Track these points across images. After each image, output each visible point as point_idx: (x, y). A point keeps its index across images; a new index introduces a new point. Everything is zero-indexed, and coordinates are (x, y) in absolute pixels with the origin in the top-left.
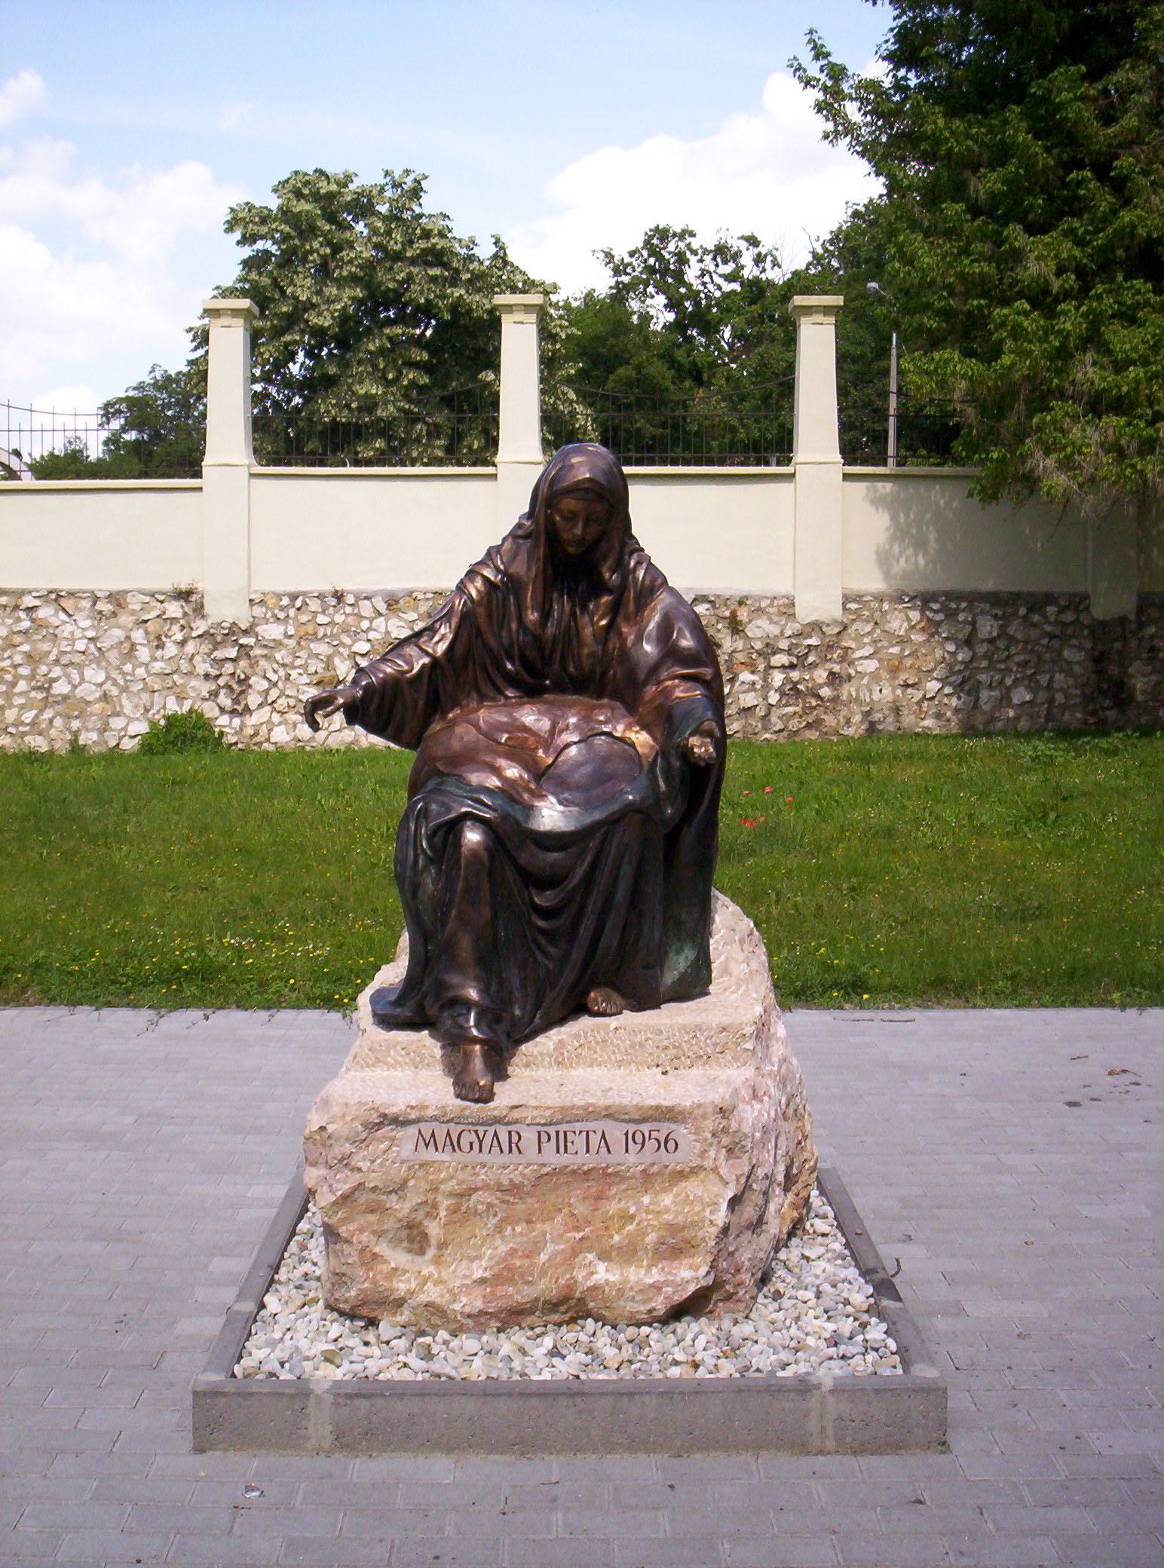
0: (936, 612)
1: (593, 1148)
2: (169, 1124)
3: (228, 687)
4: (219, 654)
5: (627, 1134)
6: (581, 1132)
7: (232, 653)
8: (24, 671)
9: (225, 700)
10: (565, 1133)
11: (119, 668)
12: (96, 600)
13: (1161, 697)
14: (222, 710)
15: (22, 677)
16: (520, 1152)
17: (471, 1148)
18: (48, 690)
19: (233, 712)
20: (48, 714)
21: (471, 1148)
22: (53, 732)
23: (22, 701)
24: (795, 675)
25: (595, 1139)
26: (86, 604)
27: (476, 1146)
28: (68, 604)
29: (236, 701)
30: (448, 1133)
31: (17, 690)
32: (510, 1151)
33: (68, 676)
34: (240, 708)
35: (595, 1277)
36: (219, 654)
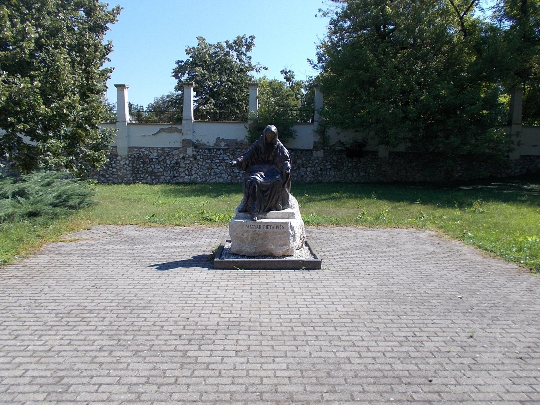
3: (187, 169)
4: (185, 162)
8: (142, 166)
9: (187, 173)
12: (158, 150)
14: (186, 175)
19: (189, 175)
20: (147, 175)
24: (313, 168)
26: (156, 151)
28: (152, 151)
36: (185, 162)
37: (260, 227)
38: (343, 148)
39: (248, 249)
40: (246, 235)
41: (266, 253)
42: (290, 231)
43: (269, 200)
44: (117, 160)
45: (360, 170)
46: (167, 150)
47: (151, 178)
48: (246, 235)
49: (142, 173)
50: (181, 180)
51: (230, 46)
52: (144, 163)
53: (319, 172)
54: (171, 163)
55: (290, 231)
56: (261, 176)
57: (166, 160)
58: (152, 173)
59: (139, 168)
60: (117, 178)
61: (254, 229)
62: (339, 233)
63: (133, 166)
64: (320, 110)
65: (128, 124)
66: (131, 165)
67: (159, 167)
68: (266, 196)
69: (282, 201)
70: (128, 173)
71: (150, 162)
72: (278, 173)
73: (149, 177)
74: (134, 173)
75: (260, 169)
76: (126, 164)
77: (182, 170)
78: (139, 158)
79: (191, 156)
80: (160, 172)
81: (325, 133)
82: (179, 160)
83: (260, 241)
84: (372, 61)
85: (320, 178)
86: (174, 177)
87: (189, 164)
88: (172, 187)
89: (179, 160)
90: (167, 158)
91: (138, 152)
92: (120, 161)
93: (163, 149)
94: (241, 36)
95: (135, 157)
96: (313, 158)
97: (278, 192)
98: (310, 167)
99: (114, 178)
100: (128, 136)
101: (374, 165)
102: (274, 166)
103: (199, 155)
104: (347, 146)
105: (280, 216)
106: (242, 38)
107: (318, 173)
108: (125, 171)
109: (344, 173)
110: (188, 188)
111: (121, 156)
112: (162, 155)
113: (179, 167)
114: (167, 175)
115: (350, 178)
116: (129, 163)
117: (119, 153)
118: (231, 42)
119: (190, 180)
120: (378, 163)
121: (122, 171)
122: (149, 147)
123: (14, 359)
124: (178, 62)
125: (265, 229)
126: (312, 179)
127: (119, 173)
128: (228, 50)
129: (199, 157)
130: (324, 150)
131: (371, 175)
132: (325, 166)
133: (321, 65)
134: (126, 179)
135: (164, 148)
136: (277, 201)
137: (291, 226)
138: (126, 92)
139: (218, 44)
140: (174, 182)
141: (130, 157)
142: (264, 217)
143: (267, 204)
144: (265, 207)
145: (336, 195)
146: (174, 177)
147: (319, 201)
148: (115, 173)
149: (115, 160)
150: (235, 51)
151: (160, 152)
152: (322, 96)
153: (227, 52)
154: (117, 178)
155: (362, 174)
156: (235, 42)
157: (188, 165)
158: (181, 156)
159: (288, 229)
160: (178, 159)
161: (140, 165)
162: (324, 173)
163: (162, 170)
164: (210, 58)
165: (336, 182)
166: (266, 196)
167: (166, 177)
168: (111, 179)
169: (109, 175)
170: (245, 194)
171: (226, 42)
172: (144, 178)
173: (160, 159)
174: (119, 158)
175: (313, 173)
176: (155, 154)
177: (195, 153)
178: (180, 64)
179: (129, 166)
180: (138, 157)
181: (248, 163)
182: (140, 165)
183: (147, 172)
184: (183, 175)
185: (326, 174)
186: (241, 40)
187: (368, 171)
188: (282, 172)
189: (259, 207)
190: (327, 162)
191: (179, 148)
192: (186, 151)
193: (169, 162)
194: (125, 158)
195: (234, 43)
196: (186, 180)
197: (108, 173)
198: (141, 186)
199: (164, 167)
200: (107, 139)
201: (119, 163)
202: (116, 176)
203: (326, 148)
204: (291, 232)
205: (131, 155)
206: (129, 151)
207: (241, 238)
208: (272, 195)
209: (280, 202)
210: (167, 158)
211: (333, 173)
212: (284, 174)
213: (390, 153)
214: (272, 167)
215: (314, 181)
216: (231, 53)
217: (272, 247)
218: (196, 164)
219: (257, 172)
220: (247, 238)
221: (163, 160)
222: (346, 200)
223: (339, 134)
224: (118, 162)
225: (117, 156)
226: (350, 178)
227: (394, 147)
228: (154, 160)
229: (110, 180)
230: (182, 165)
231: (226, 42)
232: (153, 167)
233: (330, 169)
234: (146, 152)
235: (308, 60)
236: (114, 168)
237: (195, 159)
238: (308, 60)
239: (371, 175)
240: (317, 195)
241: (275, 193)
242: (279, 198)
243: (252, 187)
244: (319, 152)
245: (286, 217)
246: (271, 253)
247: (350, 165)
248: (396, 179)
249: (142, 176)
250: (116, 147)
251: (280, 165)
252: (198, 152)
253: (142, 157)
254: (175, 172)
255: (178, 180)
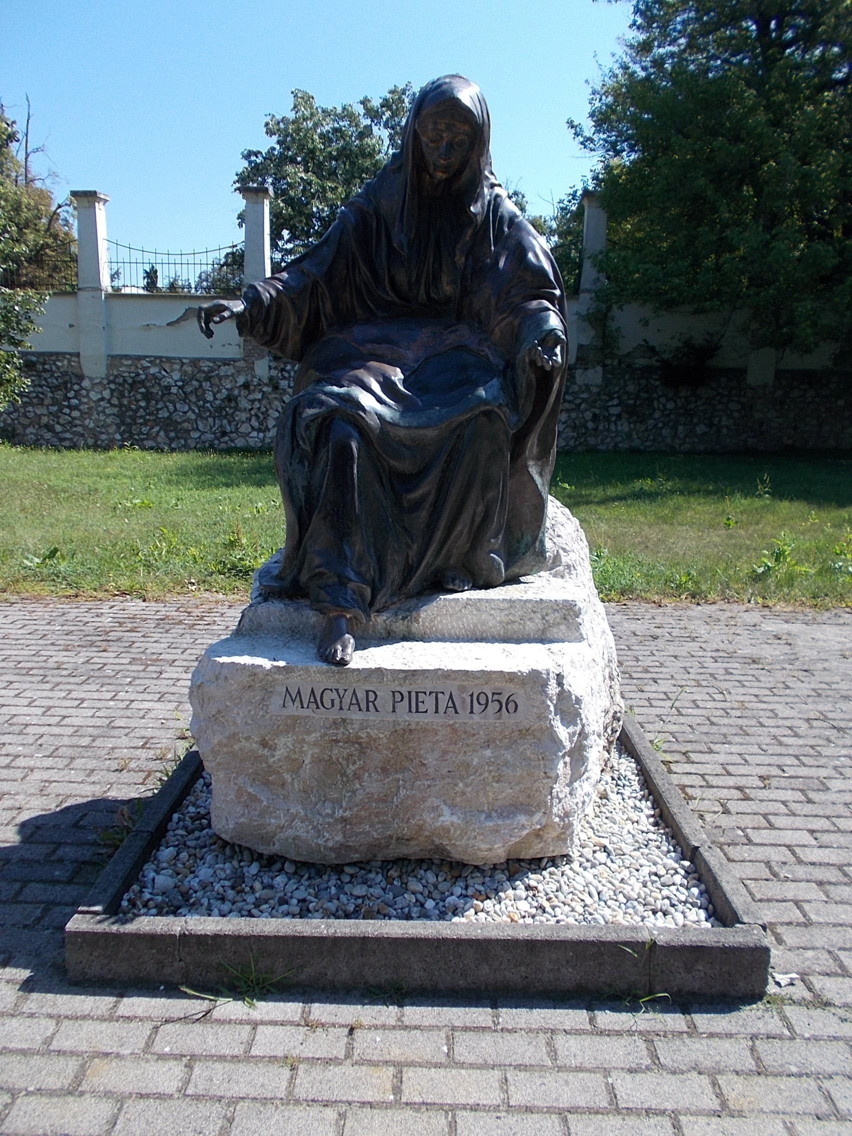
0: (656, 380)
1: (442, 709)
2: (152, 665)
3: (256, 415)
4: (251, 397)
5: (472, 695)
6: (431, 693)
7: (259, 396)
8: (143, 404)
9: (255, 423)
10: (417, 693)
11: (195, 403)
12: (183, 364)
13: (3, 956)
14: (253, 429)
15: (141, 407)
16: (377, 711)
17: (333, 706)
18: (156, 415)
19: (259, 430)
20: (156, 429)
21: (333, 706)
22: (159, 439)
23: (141, 421)
24: (573, 415)
25: (443, 700)
26: (177, 367)
27: (337, 702)
28: (167, 366)
29: (261, 423)
30: (312, 691)
31: (138, 414)
32: (368, 710)
33: (167, 407)
34: (263, 428)
35: (441, 819)
36: (251, 397)
37: (370, 702)
38: (654, 362)
39: (302, 830)
40: (284, 744)
41: (412, 850)
42: (557, 724)
43: (431, 526)
44: (82, 388)
45: (695, 420)
46: (205, 366)
47: (167, 436)
48: (284, 744)
49: (145, 424)
50: (240, 443)
51: (373, 114)
52: (148, 397)
53: (590, 425)
54: (215, 399)
55: (557, 724)
56: (388, 385)
57: (204, 393)
58: (168, 424)
59: (136, 411)
60: (82, 435)
61: (334, 714)
62: (715, 637)
63: (121, 405)
64: (600, 257)
65: (109, 296)
66: (115, 401)
67: (186, 408)
68: (417, 506)
69: (509, 531)
70: (109, 421)
71: (163, 395)
72: (487, 372)
73: (162, 433)
74: (123, 423)
75: (381, 349)
76: (103, 399)
77: (244, 416)
78: (135, 384)
79: (266, 381)
80: (188, 420)
81: (609, 323)
82: (236, 392)
83: (373, 785)
84: (753, 110)
85: (592, 441)
86: (224, 434)
87: (259, 401)
88: (211, 459)
89: (236, 392)
90: (206, 385)
91: (133, 369)
92: (88, 391)
93: (195, 362)
94: (401, 87)
95: (125, 381)
96: (575, 388)
97: (487, 485)
98: (568, 411)
99: (75, 433)
100: (108, 327)
101: (733, 406)
102: (463, 334)
103: (284, 378)
104: (665, 356)
105: (493, 622)
106: (404, 92)
107: (586, 427)
108: (102, 418)
109: (655, 425)
110: (248, 462)
111: (91, 379)
112: (193, 378)
113: (237, 408)
114: (207, 428)
115: (669, 441)
116: (112, 396)
117: (86, 372)
118: (376, 103)
119: (263, 441)
120: (743, 400)
121: (95, 416)
122: (160, 358)
123: (130, 682)
124: (248, 155)
125: (404, 716)
126: (572, 443)
127: (87, 422)
128: (368, 122)
129: (284, 384)
130: (604, 366)
131: (725, 431)
132: (606, 408)
133: (602, 136)
134: (104, 437)
135: (199, 360)
136: (477, 537)
137: (564, 695)
138: (101, 212)
139: (344, 109)
140: (223, 446)
141: (113, 382)
142: (400, 626)
143: (422, 555)
144: (409, 571)
145: (647, 484)
146: (224, 434)
147: (603, 502)
148: (78, 422)
149: (76, 387)
150: (386, 126)
151: (189, 369)
152: (603, 216)
153: (366, 127)
154: (82, 435)
155: (700, 429)
156: (386, 104)
157: (257, 405)
158: (241, 380)
159: (542, 716)
160: (231, 389)
161: (137, 401)
162: (601, 427)
163: (193, 417)
164: (324, 144)
165: (634, 451)
166: (417, 506)
167: (203, 433)
168: (68, 435)
169: (63, 425)
170: (289, 494)
171: (364, 102)
172: (148, 436)
173: (188, 389)
174: (86, 383)
175: (575, 428)
176: (176, 376)
177: (274, 373)
178: (253, 158)
179: (113, 405)
180: (134, 382)
181: (315, 315)
182: (137, 401)
183: (157, 421)
184: (245, 428)
185: (609, 430)
186: (400, 98)
187: (716, 421)
188: (510, 365)
189: (372, 573)
190: (611, 398)
191: (235, 360)
192: (253, 369)
193: (210, 397)
194: (100, 383)
195: (382, 106)
196: (252, 442)
197: (61, 421)
198: (137, 454)
199: (199, 407)
200: (18, 323)
201: (87, 396)
202: (79, 429)
203: (608, 362)
204: (563, 733)
205: (116, 377)
206: (110, 366)
207: (258, 759)
208: (442, 524)
209: (497, 542)
210: (206, 385)
211: (624, 426)
212: (525, 378)
213: (779, 374)
214: (451, 339)
215: (575, 446)
216: (375, 129)
217: (447, 818)
218: (276, 403)
219: (361, 360)
220: (295, 766)
221: (196, 389)
222: (679, 500)
223: (646, 324)
224: (84, 392)
225: (81, 377)
226: (669, 441)
227: (808, 351)
228: (174, 390)
229: (65, 439)
230: (244, 403)
231: (364, 102)
232: (171, 407)
233: (619, 416)
234: (153, 370)
235: (571, 124)
236: (76, 408)
237: (276, 388)
238: (571, 124)
239: (725, 431)
240: (596, 484)
241: (468, 487)
242: (487, 517)
243: (326, 455)
244: (590, 372)
245: (531, 627)
246: (440, 849)
247: (670, 405)
248: (790, 442)
249: (145, 429)
250: (78, 355)
251: (500, 325)
252: (283, 370)
253: (142, 382)
254: (225, 422)
255: (232, 441)
